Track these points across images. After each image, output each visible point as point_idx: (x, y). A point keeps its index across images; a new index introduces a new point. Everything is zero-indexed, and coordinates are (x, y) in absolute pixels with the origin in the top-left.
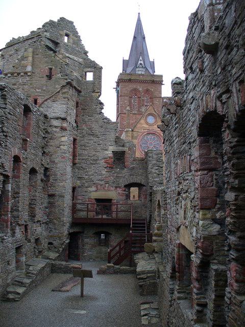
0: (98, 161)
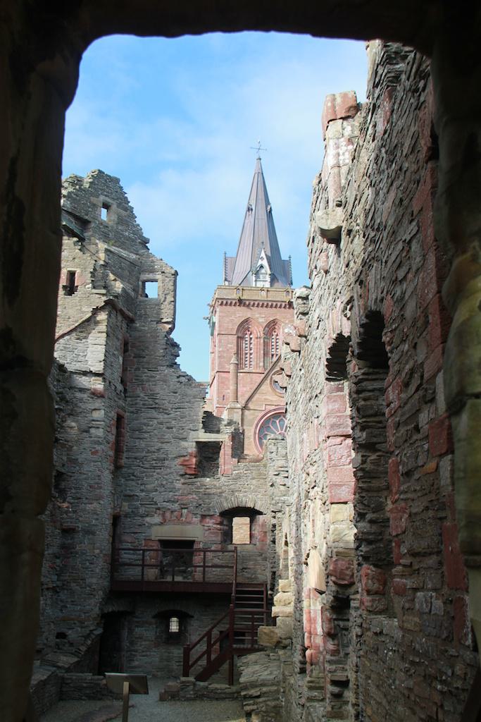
0: (167, 462)
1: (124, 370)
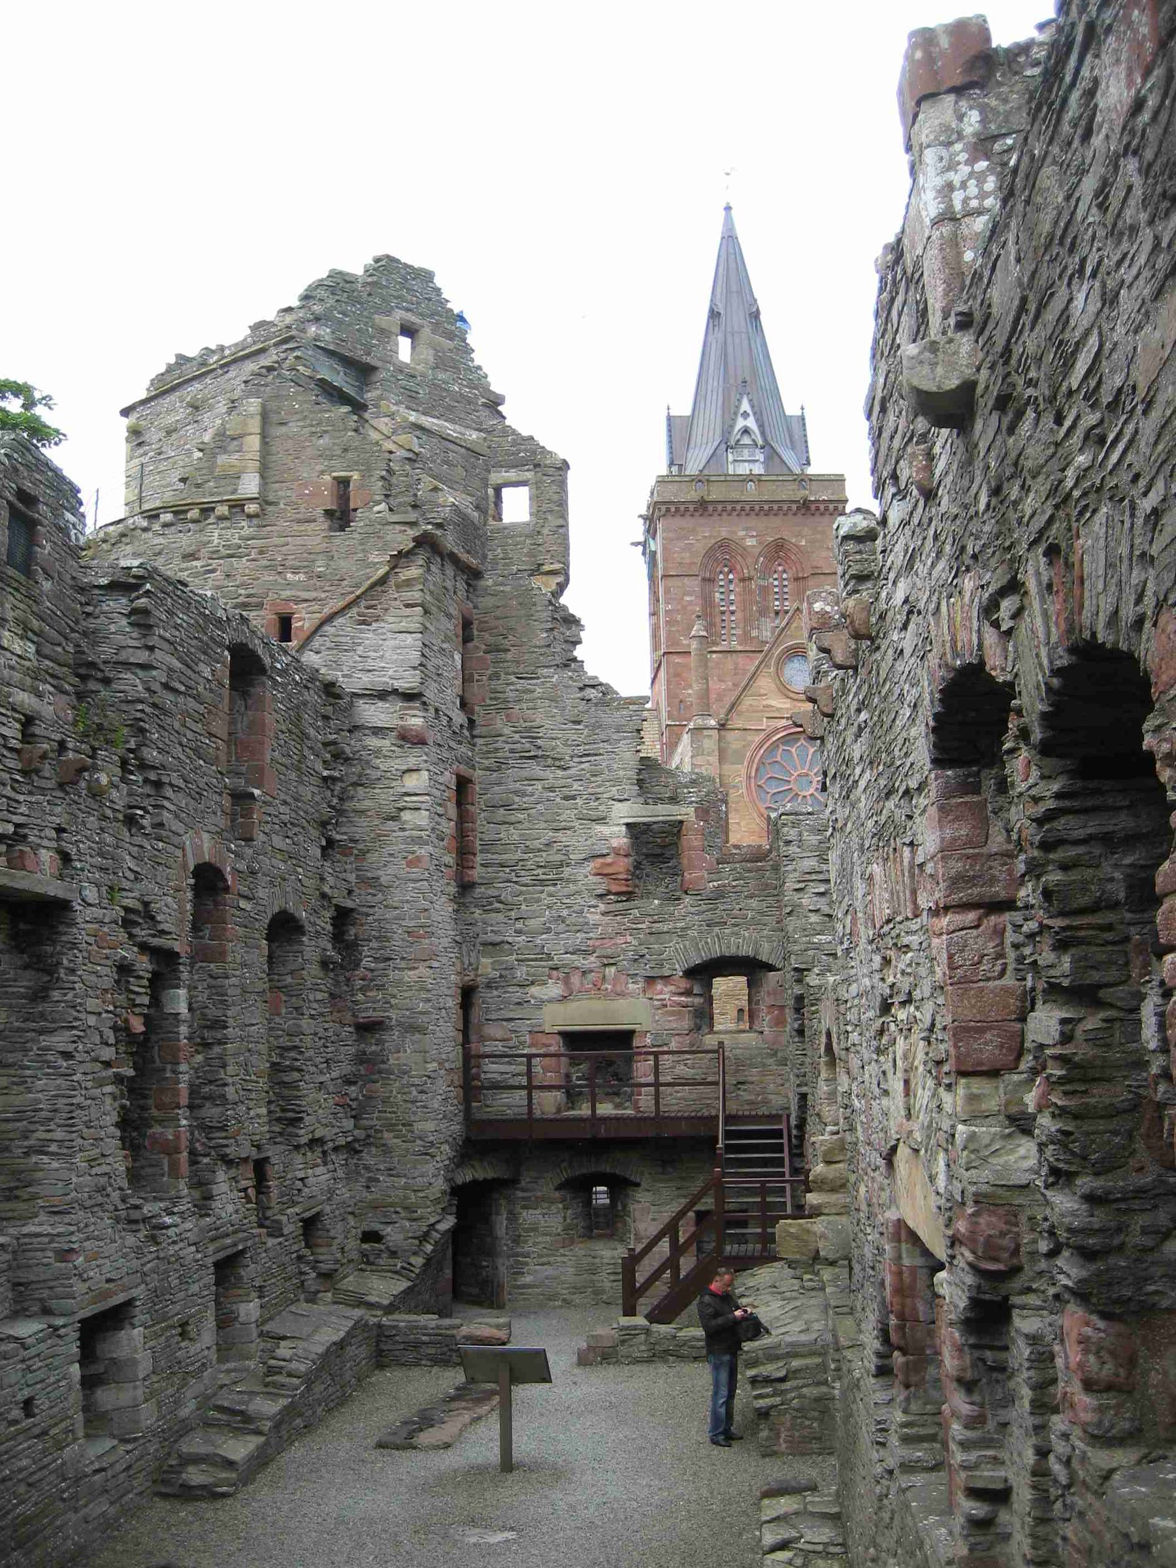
0: (567, 871)
1: (467, 680)
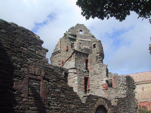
0: (99, 87)
